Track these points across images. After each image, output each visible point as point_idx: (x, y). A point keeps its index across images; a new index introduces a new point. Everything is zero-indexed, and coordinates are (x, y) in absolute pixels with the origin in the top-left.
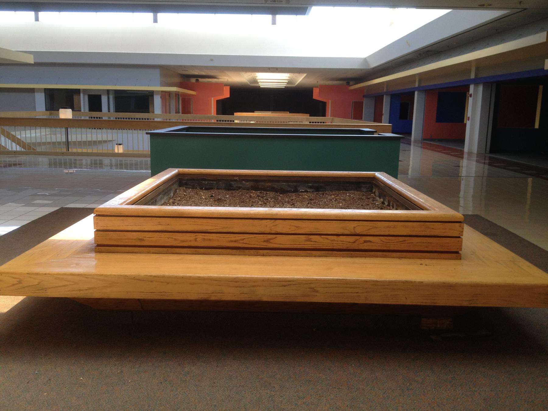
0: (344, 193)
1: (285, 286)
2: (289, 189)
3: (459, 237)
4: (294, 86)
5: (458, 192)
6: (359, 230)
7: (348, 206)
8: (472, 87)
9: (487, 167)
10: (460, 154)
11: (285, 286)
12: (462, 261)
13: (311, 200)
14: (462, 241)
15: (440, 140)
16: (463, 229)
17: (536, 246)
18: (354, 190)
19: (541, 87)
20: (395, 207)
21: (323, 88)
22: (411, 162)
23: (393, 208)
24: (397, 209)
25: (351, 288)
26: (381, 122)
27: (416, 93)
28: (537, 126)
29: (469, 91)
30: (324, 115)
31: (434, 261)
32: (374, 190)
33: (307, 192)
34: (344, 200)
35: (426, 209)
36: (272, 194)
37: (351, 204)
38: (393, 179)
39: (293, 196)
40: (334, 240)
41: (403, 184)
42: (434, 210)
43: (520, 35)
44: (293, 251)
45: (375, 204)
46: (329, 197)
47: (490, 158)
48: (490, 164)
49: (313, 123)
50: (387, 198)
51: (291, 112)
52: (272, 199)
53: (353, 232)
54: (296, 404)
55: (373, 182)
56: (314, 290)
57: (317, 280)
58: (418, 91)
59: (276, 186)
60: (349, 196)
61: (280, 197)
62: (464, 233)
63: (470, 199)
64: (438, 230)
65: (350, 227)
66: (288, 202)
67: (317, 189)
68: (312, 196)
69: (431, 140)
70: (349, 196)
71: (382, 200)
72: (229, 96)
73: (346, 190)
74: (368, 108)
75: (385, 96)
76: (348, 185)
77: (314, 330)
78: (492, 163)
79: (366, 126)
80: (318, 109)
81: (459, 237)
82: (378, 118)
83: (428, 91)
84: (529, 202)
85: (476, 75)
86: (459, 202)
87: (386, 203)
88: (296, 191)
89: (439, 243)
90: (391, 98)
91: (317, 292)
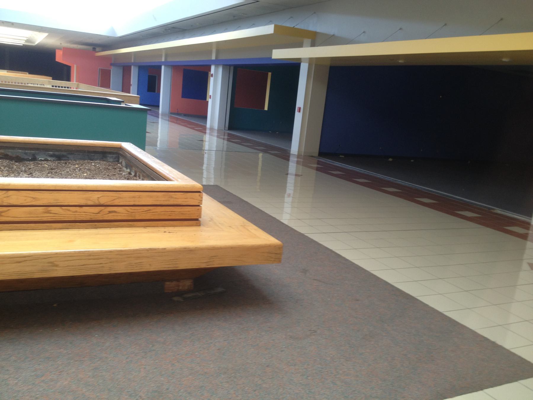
0: (88, 163)
1: (20, 262)
2: (26, 157)
3: (199, 206)
4: (34, 45)
5: (202, 164)
6: (103, 201)
7: (93, 177)
8: (213, 68)
9: (226, 142)
10: (203, 130)
11: (20, 262)
12: (202, 228)
13: (52, 169)
14: (201, 209)
15: (185, 115)
16: (202, 198)
17: (264, 212)
18: (100, 160)
19: (270, 74)
20: (141, 178)
21: (66, 50)
22: (159, 135)
23: (140, 178)
24: (143, 180)
25: (94, 259)
26: (129, 93)
27: (163, 67)
28: (266, 108)
29: (210, 71)
30: (68, 79)
31: (177, 229)
32: (120, 161)
33: (46, 160)
34: (89, 170)
35: (170, 180)
36: (6, 162)
37: (96, 174)
38: (139, 150)
39: (31, 165)
40: (76, 212)
41: (149, 155)
42: (177, 181)
43: (254, 24)
44: (51, 224)
45: (121, 174)
46: (72, 167)
47: (229, 135)
48: (228, 140)
49: (56, 87)
50: (134, 168)
51: (30, 73)
52: (5, 167)
53: (97, 203)
54: (34, 384)
55: (118, 154)
56: (53, 264)
57: (56, 254)
58: (165, 66)
59: (10, 154)
60: (94, 166)
61: (16, 165)
62: (204, 202)
63: (212, 171)
64: (180, 199)
65: (94, 198)
66: (25, 171)
67: (59, 158)
68: (53, 165)
69: (178, 114)
70: (94, 166)
71: (129, 170)
72: (57, 60)
73: (92, 160)
74: (116, 76)
75: (132, 67)
76: (92, 154)
77: (55, 305)
78: (231, 138)
79: (113, 94)
80: (61, 72)
81: (199, 206)
82: (126, 88)
83: (175, 67)
84: (259, 174)
85: (216, 57)
86: (202, 173)
87: (133, 174)
88: (34, 159)
89: (180, 212)
90: (123, 69)
91: (57, 266)
